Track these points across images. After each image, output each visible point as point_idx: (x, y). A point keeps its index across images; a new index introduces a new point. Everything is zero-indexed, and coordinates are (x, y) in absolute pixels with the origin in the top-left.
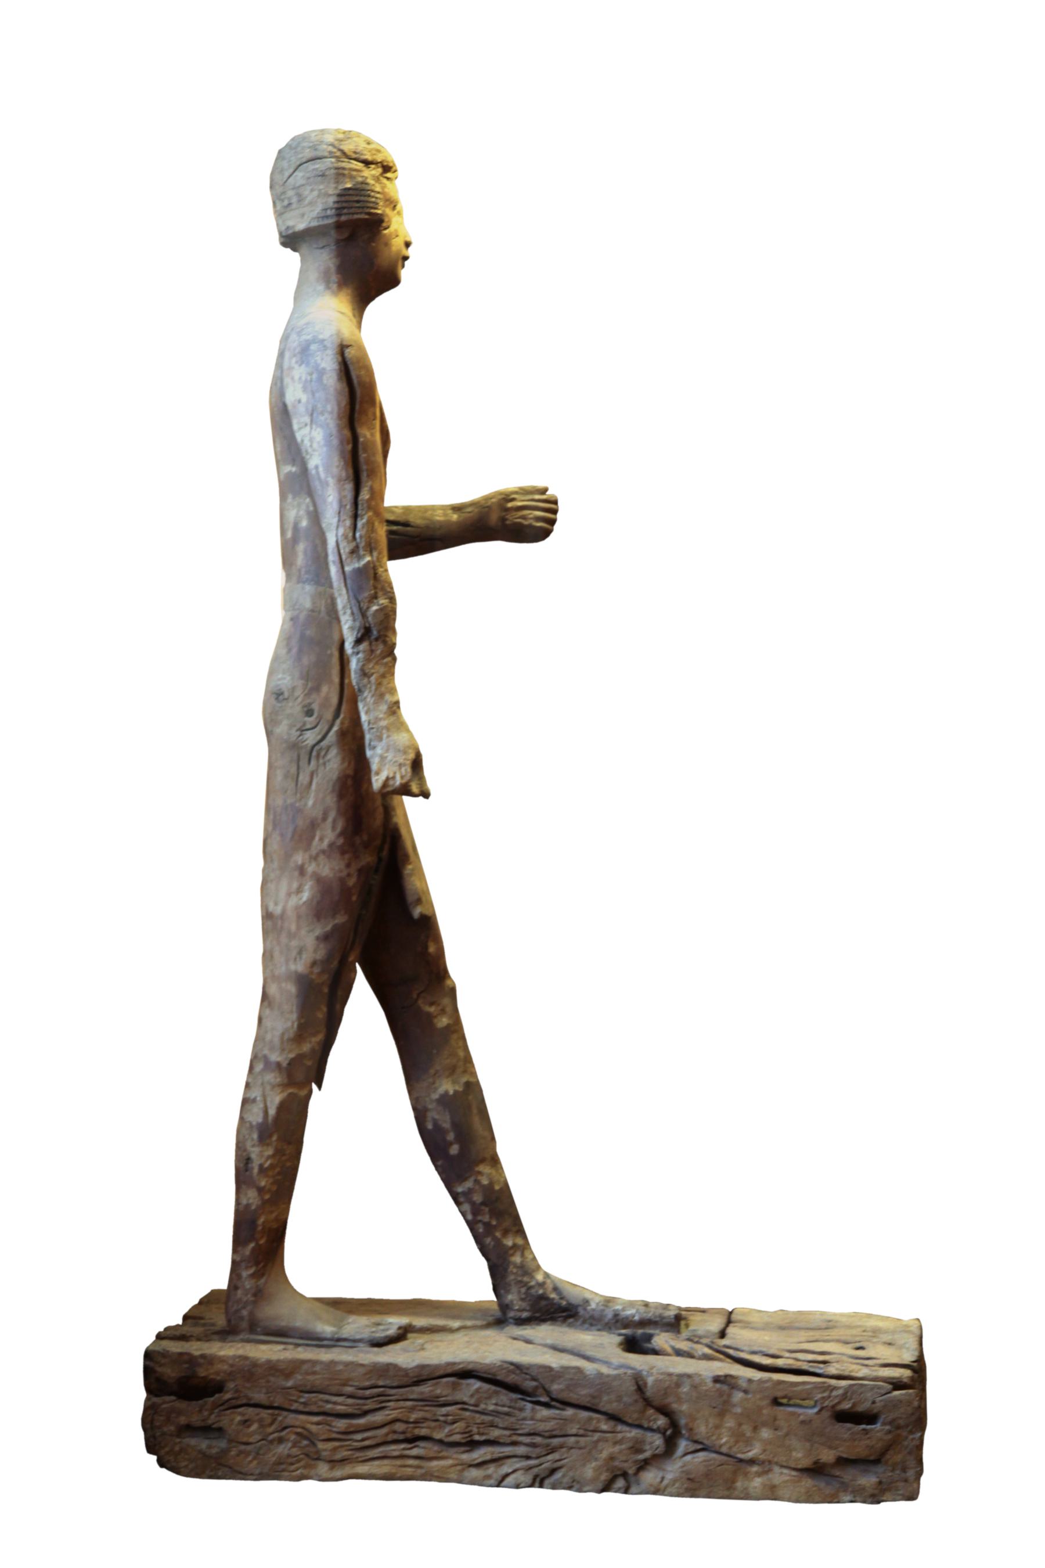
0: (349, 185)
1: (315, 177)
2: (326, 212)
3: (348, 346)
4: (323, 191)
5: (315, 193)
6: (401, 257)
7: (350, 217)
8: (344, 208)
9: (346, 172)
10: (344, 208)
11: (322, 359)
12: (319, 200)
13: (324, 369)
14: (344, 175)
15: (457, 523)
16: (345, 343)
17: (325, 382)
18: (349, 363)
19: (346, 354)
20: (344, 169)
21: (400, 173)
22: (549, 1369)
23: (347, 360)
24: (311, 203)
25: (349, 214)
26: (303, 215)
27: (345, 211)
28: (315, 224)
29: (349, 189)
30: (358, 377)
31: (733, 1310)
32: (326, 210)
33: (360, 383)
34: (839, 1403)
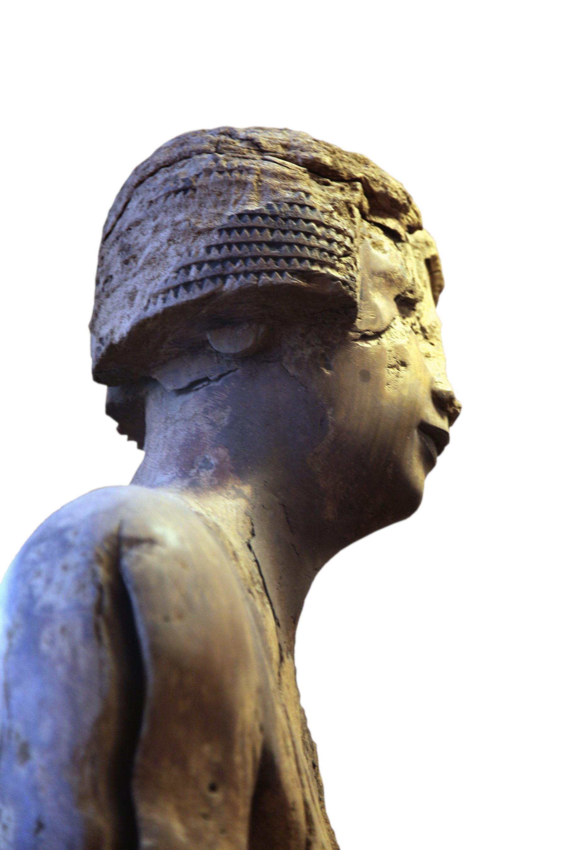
0: (253, 207)
1: (167, 195)
2: (188, 273)
3: (136, 542)
4: (184, 225)
5: (164, 235)
6: (415, 422)
7: (252, 279)
8: (234, 260)
9: (252, 178)
10: (234, 260)
11: (49, 581)
12: (171, 251)
13: (49, 609)
14: (243, 184)
16: (127, 532)
17: (44, 647)
18: (129, 587)
19: (126, 562)
20: (249, 170)
21: (418, 202)
23: (127, 576)
24: (151, 262)
25: (246, 274)
26: (132, 296)
27: (238, 266)
28: (158, 307)
29: (252, 215)
30: (153, 631)
32: (187, 268)
33: (154, 647)
34: (413, 209)
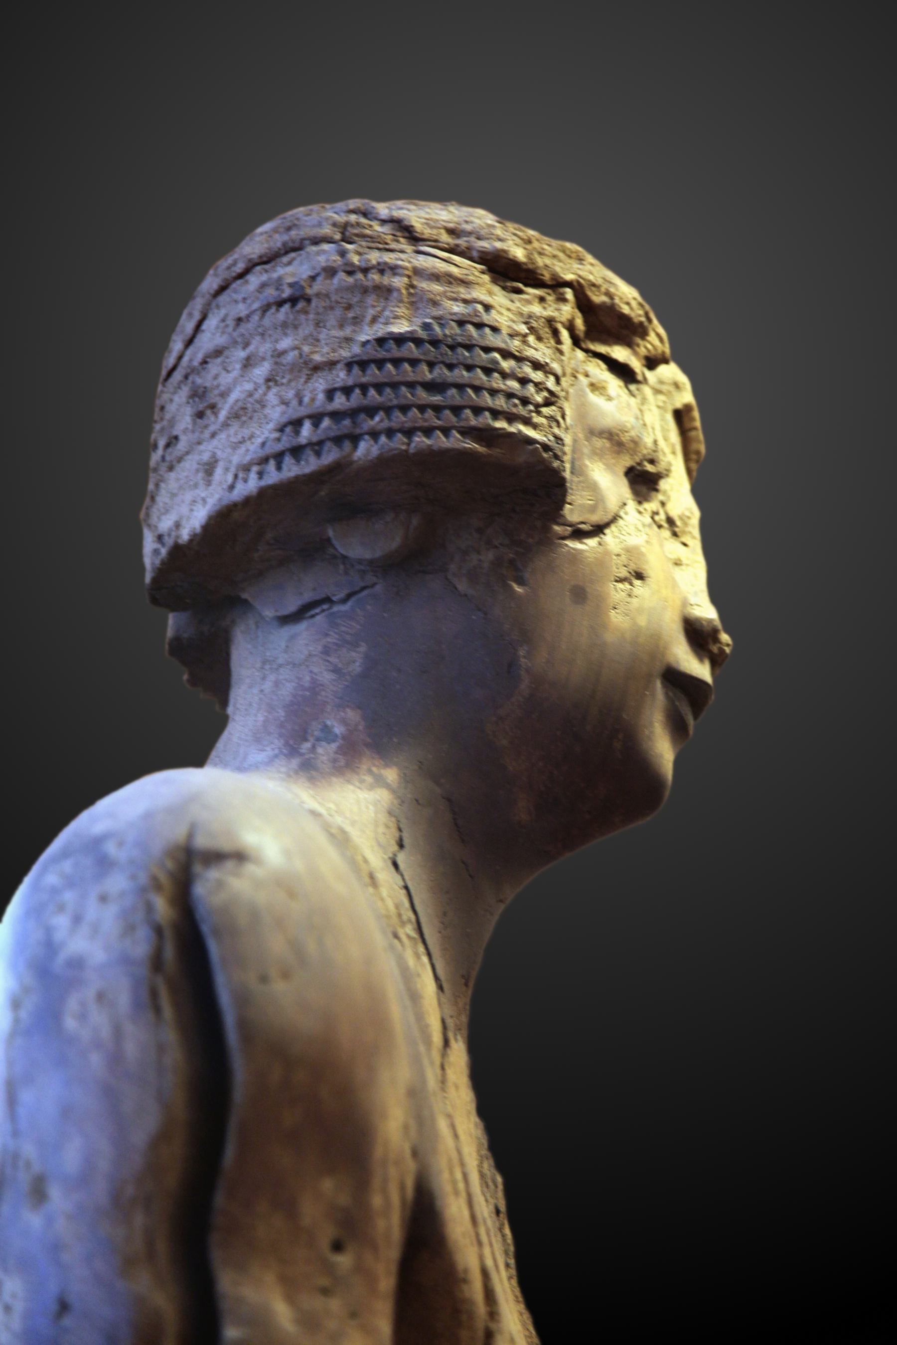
0: (401, 327)
1: (265, 309)
2: (297, 433)
3: (215, 857)
4: (291, 356)
6: (658, 668)
7: (399, 442)
8: (371, 411)
9: (399, 282)
10: (371, 411)
11: (77, 919)
12: (272, 397)
13: (77, 963)
14: (386, 292)
15: (243, 244)
16: (201, 842)
17: (70, 1023)
18: (205, 929)
19: (200, 890)
20: (394, 269)
22: (440, 405)
23: (201, 912)
24: (239, 414)
25: (390, 433)
27: (378, 421)
28: (251, 485)
29: (400, 340)
30: (243, 999)
31: (443, 798)
32: (297, 424)
33: (244, 1024)
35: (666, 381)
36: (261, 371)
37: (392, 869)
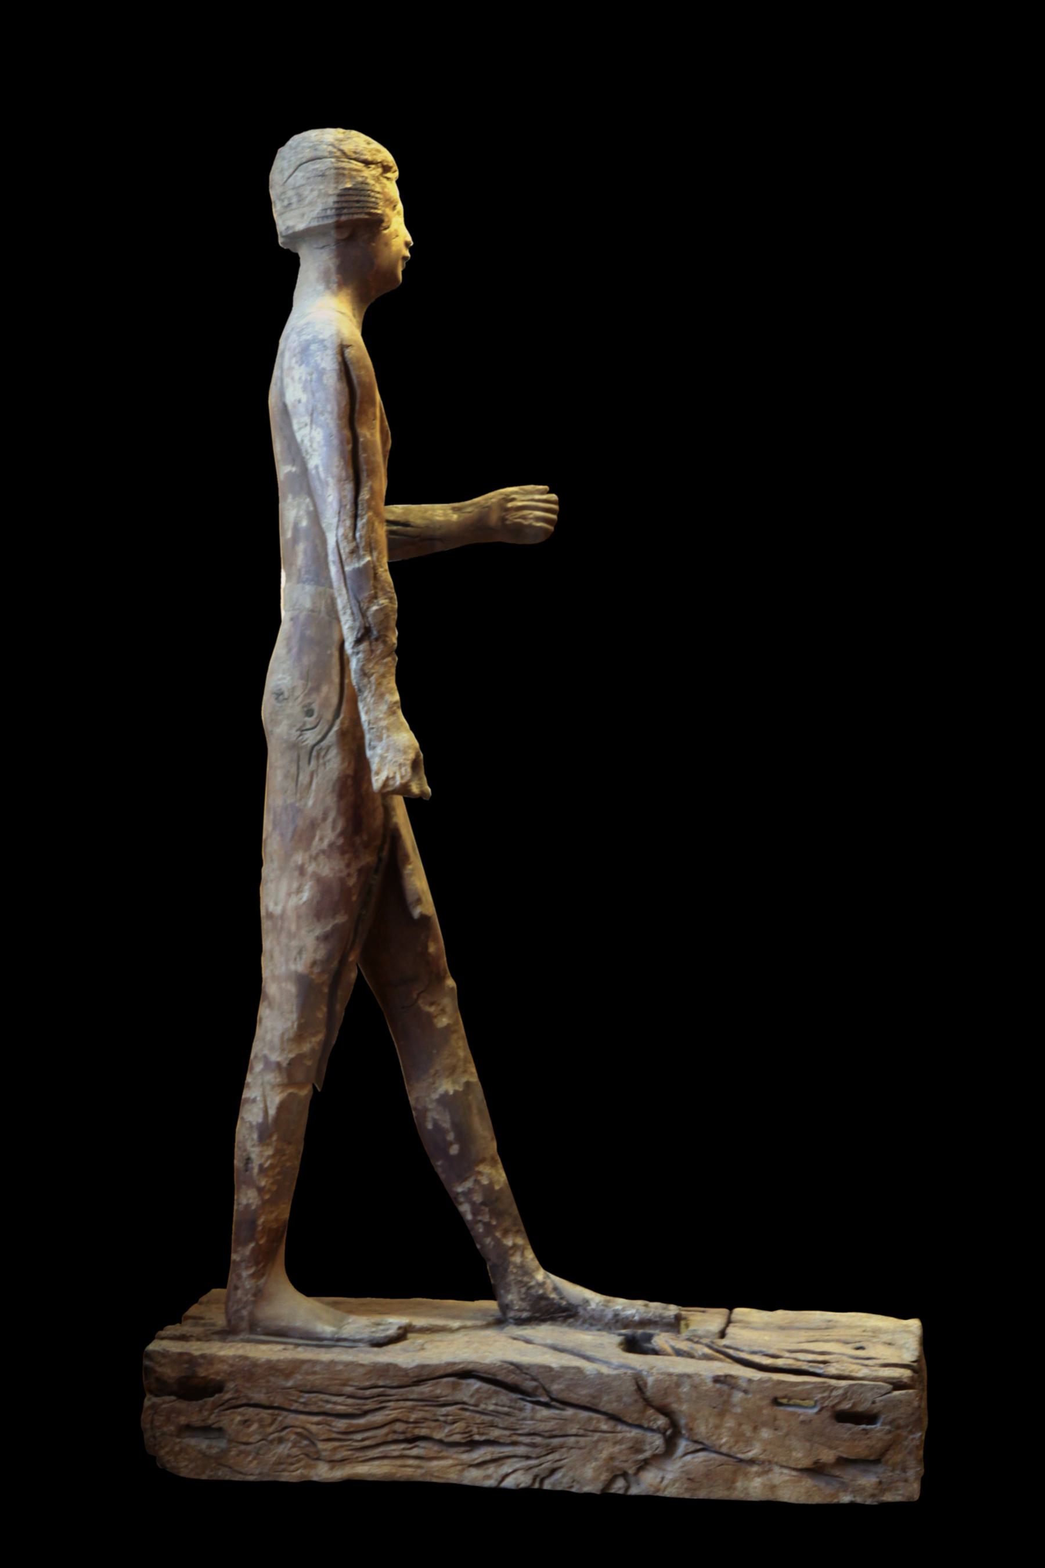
0: (349, 185)
1: (315, 177)
2: (326, 212)
3: (348, 346)
4: (323, 191)
6: (401, 257)
7: (350, 217)
8: (344, 208)
9: (346, 172)
10: (344, 208)
11: (322, 359)
12: (319, 200)
13: (324, 369)
14: (344, 175)
16: (345, 343)
17: (325, 382)
18: (349, 363)
19: (346, 354)
20: (344, 169)
23: (347, 360)
24: (311, 203)
25: (349, 214)
26: (303, 215)
27: (345, 211)
29: (349, 189)
30: (358, 377)
32: (326, 210)
33: (360, 383)
34: (839, 1403)
35: (868, 1329)
36: (315, 193)
37: (890, 1346)
